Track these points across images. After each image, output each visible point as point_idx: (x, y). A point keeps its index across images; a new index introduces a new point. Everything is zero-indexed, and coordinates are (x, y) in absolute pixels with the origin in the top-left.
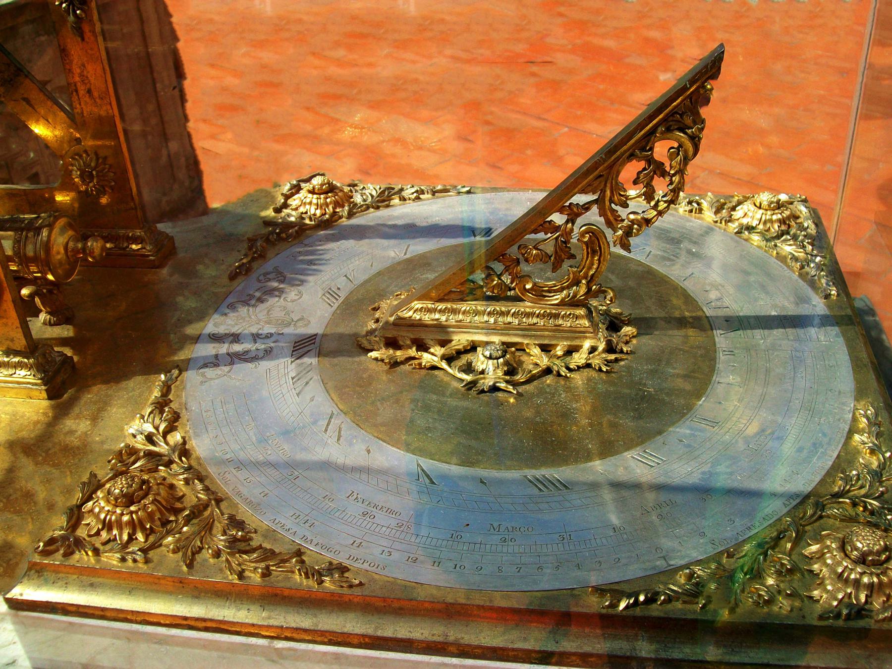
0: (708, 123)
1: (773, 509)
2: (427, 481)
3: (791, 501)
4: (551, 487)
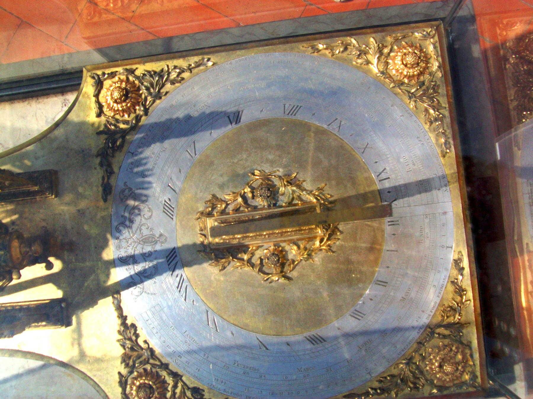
0: (11, 339)
1: (414, 335)
2: (264, 349)
3: (421, 330)
4: (318, 342)
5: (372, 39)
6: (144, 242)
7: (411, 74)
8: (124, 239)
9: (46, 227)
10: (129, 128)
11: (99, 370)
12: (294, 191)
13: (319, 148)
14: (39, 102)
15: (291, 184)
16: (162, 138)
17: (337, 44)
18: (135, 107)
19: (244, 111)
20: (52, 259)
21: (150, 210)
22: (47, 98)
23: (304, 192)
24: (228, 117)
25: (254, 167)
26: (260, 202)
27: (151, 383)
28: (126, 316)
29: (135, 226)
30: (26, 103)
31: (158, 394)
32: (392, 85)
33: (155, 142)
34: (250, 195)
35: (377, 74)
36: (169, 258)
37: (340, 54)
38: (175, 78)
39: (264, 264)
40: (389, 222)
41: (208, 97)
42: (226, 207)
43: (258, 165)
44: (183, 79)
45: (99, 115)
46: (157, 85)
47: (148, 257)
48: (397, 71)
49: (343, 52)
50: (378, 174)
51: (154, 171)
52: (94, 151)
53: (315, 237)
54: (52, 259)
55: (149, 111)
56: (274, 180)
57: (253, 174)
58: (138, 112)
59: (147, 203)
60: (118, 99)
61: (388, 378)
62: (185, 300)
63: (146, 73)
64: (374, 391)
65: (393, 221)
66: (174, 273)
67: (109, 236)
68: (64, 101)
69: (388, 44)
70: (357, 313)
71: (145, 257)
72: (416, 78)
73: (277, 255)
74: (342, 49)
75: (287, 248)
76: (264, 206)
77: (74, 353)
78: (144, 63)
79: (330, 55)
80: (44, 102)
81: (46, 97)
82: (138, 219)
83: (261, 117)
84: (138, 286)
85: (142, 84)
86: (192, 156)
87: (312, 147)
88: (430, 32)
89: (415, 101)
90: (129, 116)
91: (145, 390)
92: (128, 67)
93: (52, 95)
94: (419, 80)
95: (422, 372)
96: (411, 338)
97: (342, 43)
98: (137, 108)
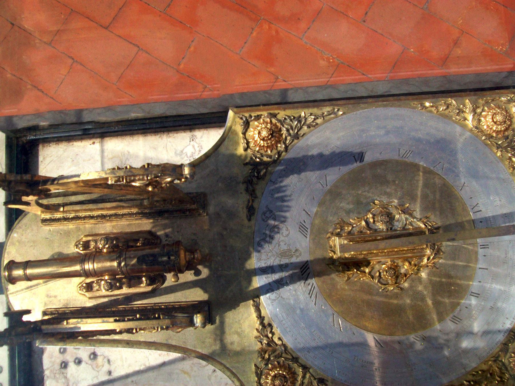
5: (467, 101)
6: (282, 256)
7: (499, 129)
8: (265, 252)
9: (196, 240)
10: (271, 161)
11: (238, 362)
12: (406, 219)
13: (426, 185)
14: (170, 137)
15: (404, 213)
16: (299, 171)
17: (440, 103)
18: (277, 144)
19: (367, 153)
20: (200, 267)
21: (287, 230)
22: (177, 133)
23: (415, 220)
24: (354, 157)
25: (375, 198)
26: (381, 226)
27: (284, 373)
28: (264, 317)
29: (274, 242)
30: (157, 137)
31: (290, 383)
32: (483, 138)
33: (292, 174)
34: (371, 220)
35: (472, 128)
36: (302, 269)
37: (443, 112)
38: (310, 123)
39: (382, 276)
40: (481, 246)
41: (338, 139)
42: (351, 230)
43: (378, 196)
44: (317, 124)
45: (246, 150)
46: (295, 128)
47: (285, 268)
48: (488, 126)
49: (445, 109)
50: (472, 207)
51: (292, 197)
52: (241, 179)
53: (424, 256)
54: (200, 267)
55: (289, 148)
56: (391, 209)
57: (374, 203)
58: (279, 149)
59: (285, 224)
60: (265, 137)
61: (480, 372)
62: (315, 304)
63: (287, 117)
64: (468, 383)
65: (484, 245)
66: (307, 282)
67: (251, 249)
68: (191, 137)
69: (481, 105)
70: (455, 318)
71: (282, 268)
72: (502, 133)
73: (394, 269)
74: (444, 108)
75: (400, 264)
76: (383, 229)
77: (217, 347)
78: (285, 109)
79: (435, 112)
80: (174, 136)
81: (176, 132)
82: (277, 236)
83: (381, 157)
84: (275, 292)
85: (283, 126)
86: (324, 187)
87: (421, 183)
88: (513, 97)
89: (501, 151)
90: (271, 152)
91: (281, 379)
92: (272, 112)
93: (182, 131)
94: (504, 135)
95: (506, 369)
96: (497, 340)
97: (445, 103)
98: (279, 145)
